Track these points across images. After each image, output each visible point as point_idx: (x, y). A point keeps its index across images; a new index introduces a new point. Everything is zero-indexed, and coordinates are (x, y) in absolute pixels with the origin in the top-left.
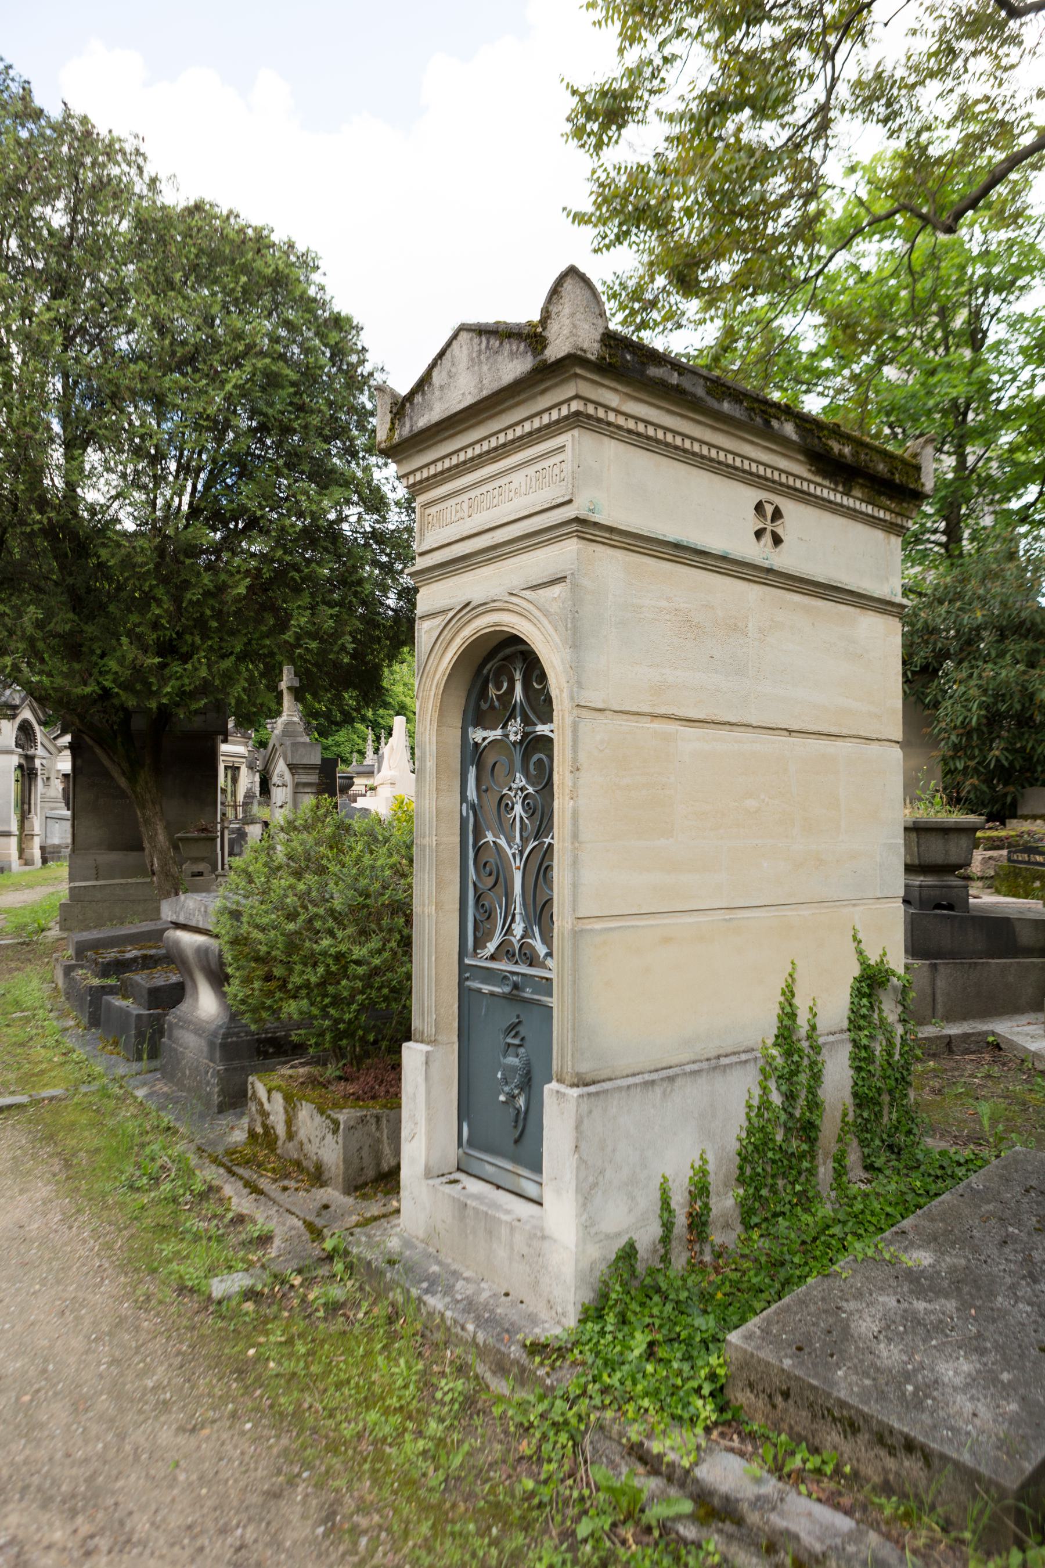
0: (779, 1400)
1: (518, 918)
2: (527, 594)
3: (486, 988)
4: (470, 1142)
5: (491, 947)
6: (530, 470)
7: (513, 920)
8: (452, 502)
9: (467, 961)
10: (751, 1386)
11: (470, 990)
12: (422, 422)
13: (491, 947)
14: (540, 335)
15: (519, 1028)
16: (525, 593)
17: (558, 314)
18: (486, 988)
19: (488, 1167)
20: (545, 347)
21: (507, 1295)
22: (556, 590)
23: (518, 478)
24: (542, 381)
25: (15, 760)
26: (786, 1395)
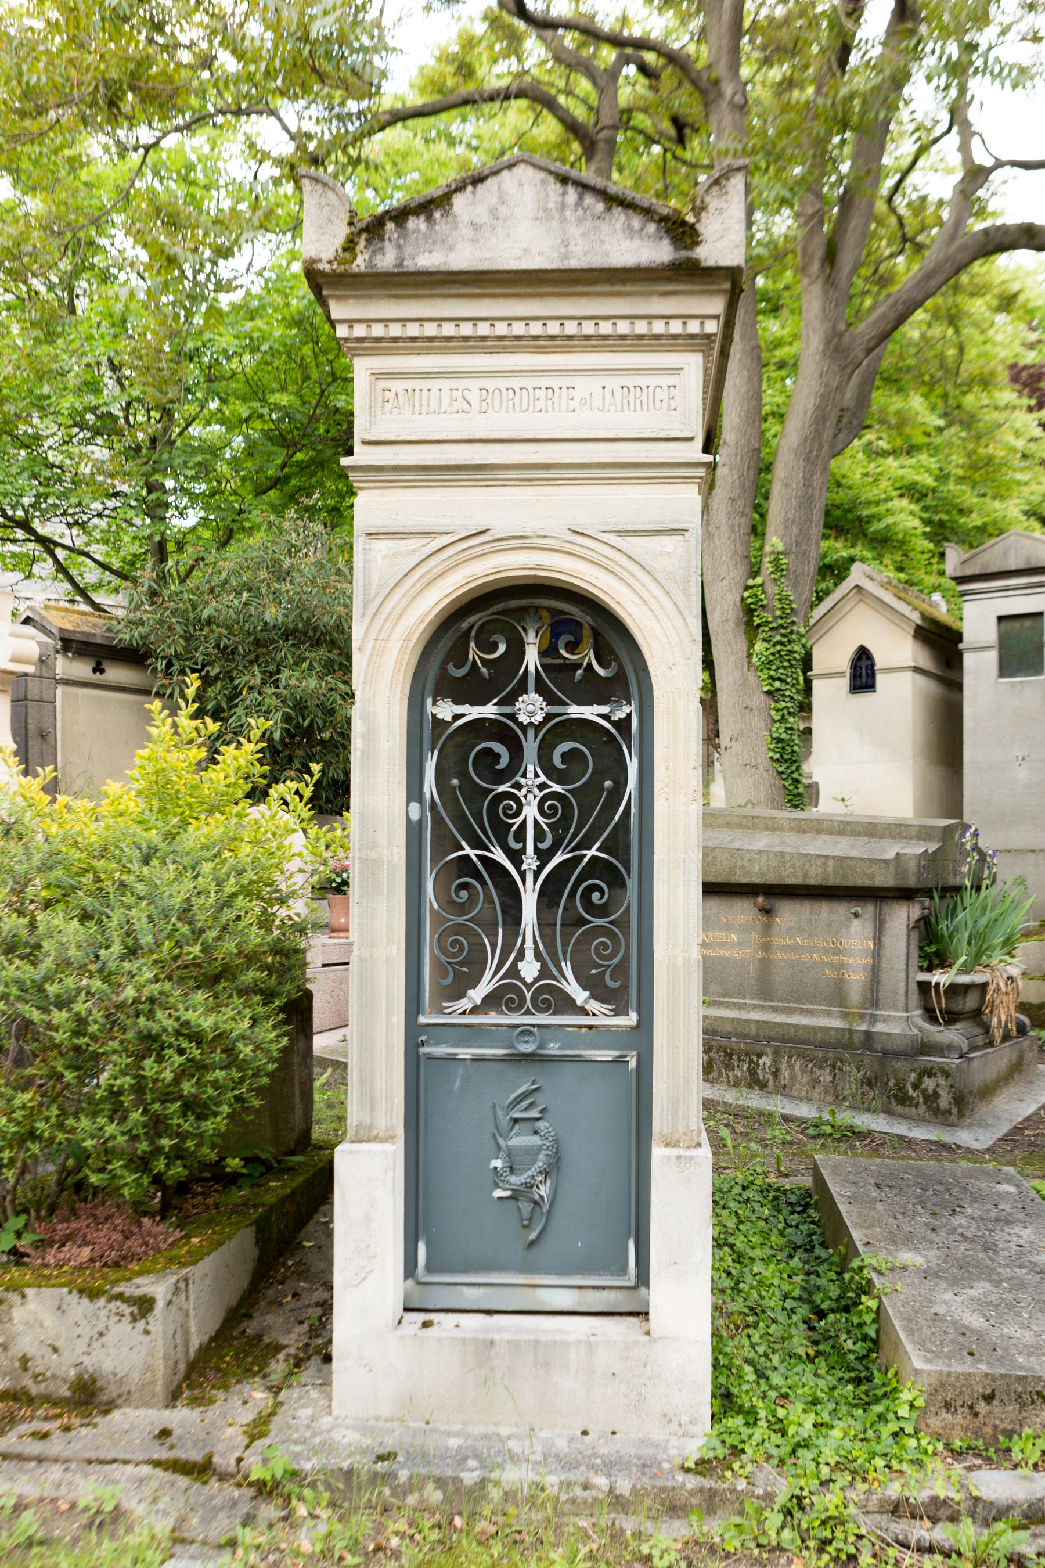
0: (982, 1407)
1: (529, 954)
2: (612, 539)
3: (465, 1053)
4: (430, 1269)
5: (477, 995)
6: (614, 382)
7: (521, 956)
8: (445, 384)
9: (423, 1020)
10: (947, 1406)
11: (430, 1058)
12: (427, 260)
13: (477, 995)
14: (692, 226)
15: (537, 1097)
16: (605, 537)
17: (721, 211)
18: (465, 1053)
19: (468, 1291)
20: (698, 244)
21: (585, 1433)
22: (669, 543)
23: (584, 385)
24: (676, 281)
25: (815, 671)
26: (989, 1398)
